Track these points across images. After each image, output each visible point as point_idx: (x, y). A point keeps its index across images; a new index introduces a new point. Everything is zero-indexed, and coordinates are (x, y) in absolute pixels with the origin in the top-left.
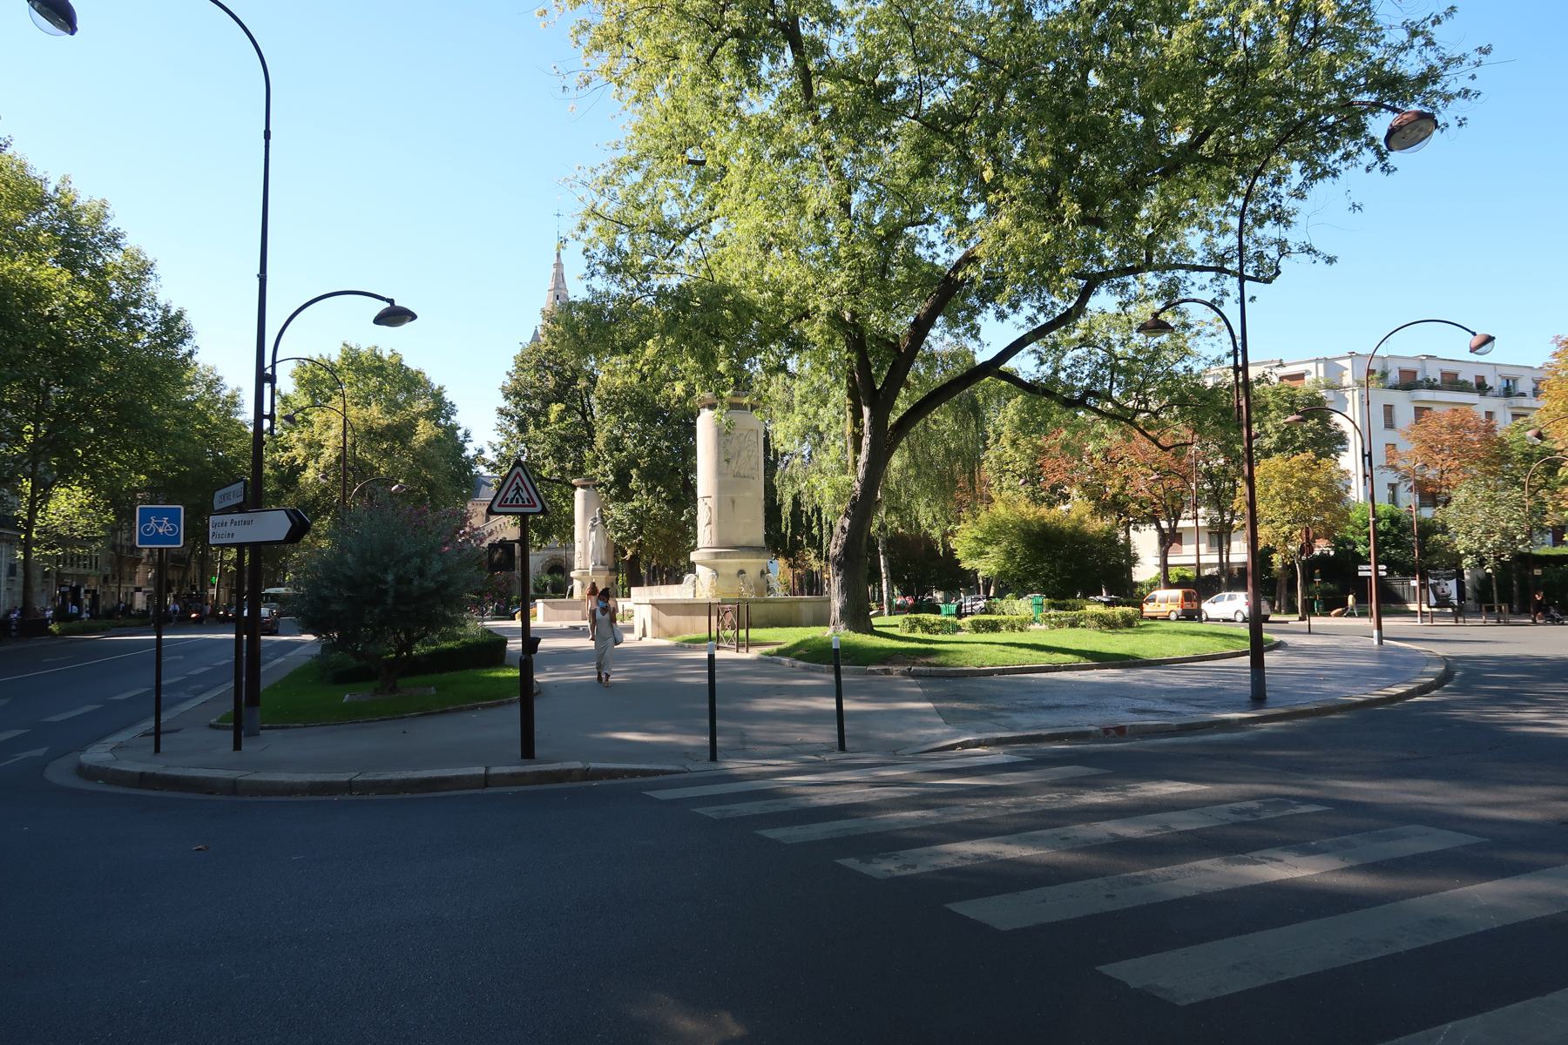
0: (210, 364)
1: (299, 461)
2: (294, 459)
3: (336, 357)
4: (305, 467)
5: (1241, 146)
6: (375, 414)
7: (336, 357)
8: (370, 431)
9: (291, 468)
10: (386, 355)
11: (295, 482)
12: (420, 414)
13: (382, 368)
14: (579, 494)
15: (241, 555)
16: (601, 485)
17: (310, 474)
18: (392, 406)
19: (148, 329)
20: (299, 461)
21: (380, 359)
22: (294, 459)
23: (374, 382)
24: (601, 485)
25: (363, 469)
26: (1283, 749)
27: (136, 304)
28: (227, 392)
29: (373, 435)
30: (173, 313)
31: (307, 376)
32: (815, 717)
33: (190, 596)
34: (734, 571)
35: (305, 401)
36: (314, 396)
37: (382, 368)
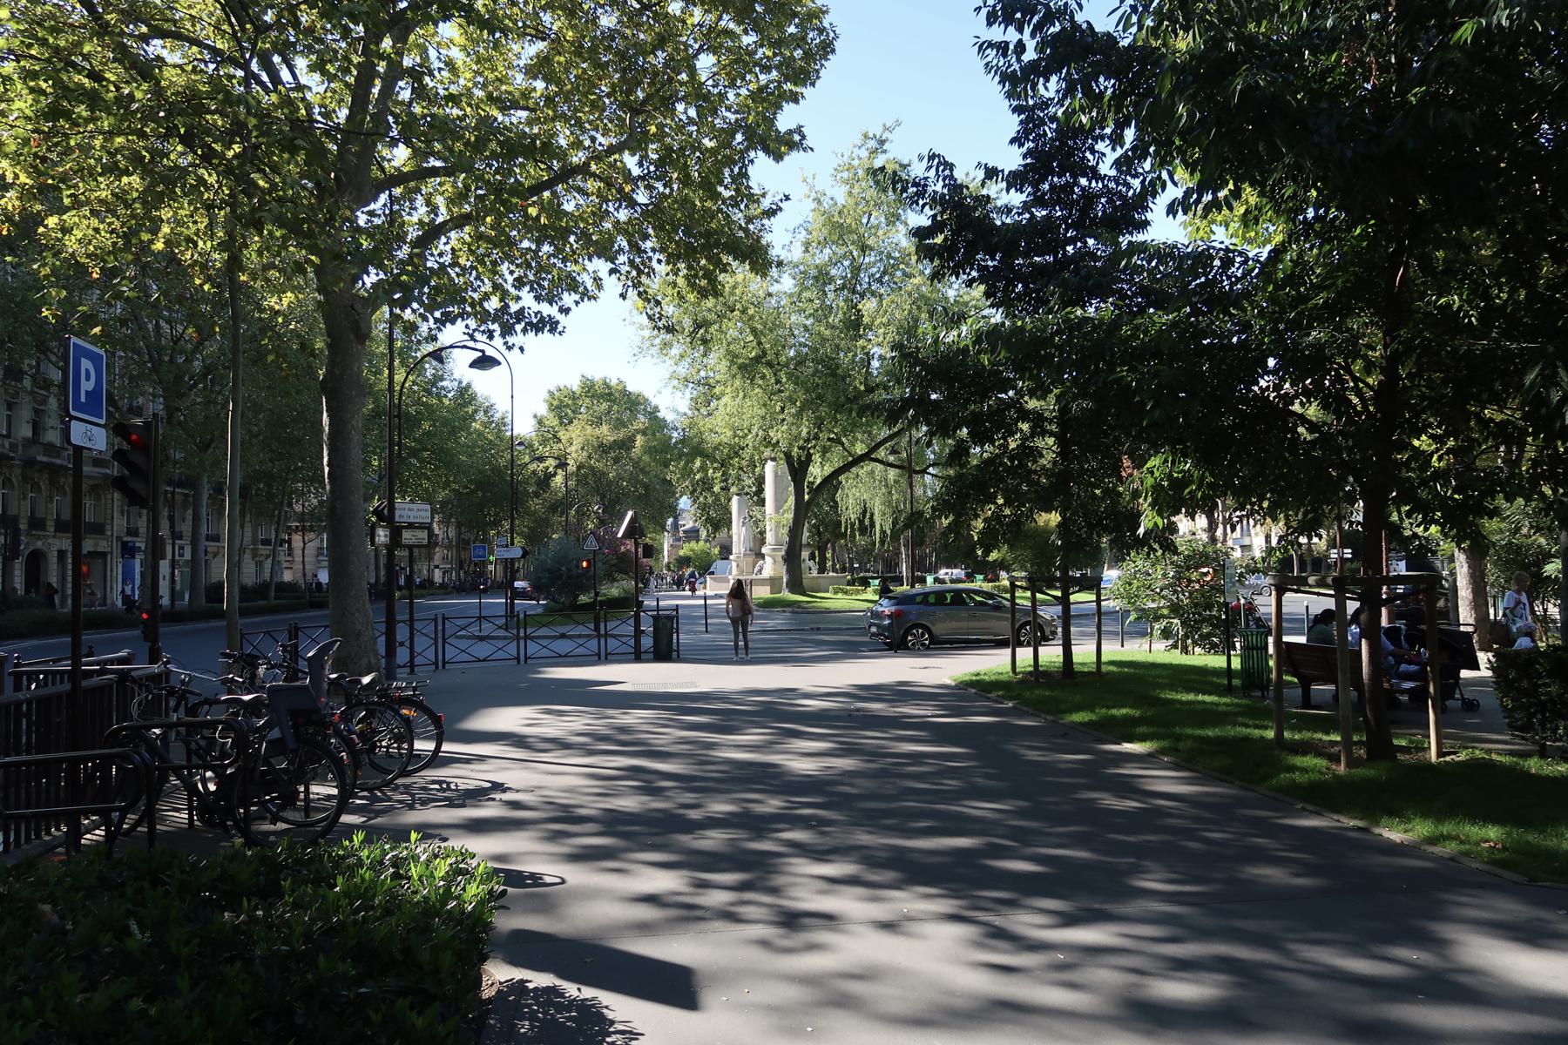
0: (486, 393)
1: (551, 469)
2: (547, 468)
3: (575, 385)
4: (555, 474)
5: (829, 397)
6: (606, 432)
7: (575, 385)
8: (601, 445)
9: (546, 474)
10: (614, 382)
11: (548, 485)
12: (638, 431)
13: (610, 394)
14: (735, 499)
15: (1449, 737)
16: (747, 494)
17: (559, 479)
18: (619, 424)
19: (450, 395)
20: (551, 469)
21: (609, 387)
22: (547, 468)
23: (605, 406)
24: (747, 494)
25: (599, 476)
26: (1188, 690)
27: (442, 379)
28: (498, 416)
29: (603, 449)
30: (464, 384)
31: (555, 403)
32: (699, 606)
33: (475, 572)
34: (40, 514)
35: (556, 422)
36: (561, 418)
37: (610, 394)
